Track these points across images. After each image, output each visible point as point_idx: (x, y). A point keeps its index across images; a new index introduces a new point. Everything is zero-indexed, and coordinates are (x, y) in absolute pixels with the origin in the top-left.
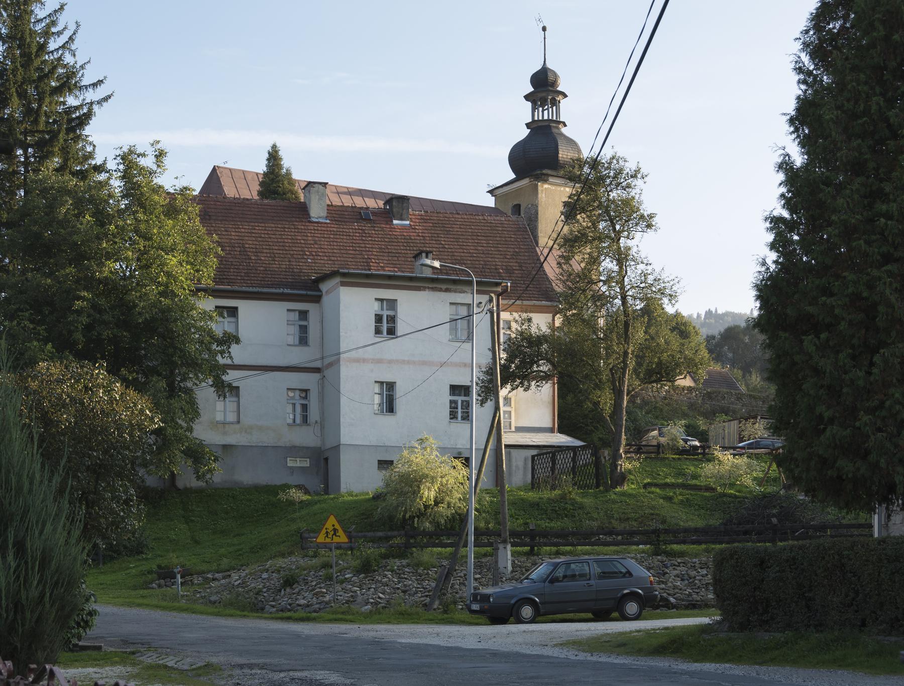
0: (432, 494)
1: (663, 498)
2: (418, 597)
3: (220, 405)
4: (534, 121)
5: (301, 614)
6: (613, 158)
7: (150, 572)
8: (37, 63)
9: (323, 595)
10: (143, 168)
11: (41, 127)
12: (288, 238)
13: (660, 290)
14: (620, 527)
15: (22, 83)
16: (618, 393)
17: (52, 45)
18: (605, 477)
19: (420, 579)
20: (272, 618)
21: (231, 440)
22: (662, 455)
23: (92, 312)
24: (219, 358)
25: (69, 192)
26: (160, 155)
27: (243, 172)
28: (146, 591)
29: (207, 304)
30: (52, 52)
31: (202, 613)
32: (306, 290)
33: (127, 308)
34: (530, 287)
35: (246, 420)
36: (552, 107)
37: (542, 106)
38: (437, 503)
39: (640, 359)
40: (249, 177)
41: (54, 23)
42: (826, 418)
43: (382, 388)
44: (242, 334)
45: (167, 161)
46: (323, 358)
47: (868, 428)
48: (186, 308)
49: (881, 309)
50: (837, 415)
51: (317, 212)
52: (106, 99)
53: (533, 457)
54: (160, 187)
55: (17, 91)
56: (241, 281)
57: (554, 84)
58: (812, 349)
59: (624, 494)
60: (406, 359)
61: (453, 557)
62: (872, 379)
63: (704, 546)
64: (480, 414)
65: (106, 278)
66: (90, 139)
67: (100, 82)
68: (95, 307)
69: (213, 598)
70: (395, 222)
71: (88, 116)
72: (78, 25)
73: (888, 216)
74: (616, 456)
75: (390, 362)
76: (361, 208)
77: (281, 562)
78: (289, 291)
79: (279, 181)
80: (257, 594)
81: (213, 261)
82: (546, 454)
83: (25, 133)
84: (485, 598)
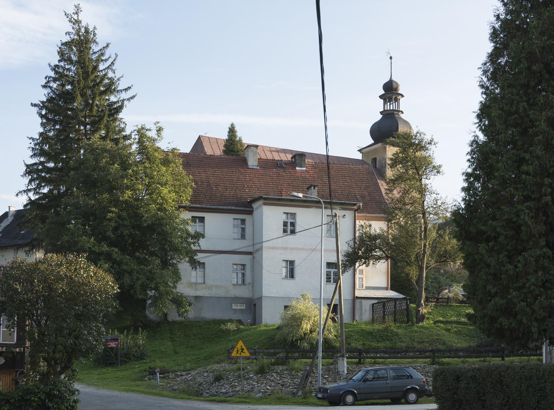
0: (309, 327)
1: (445, 330)
2: (290, 389)
3: (194, 273)
4: (384, 110)
5: (222, 398)
6: (417, 133)
7: (145, 371)
8: (92, 77)
9: (236, 387)
10: (149, 137)
11: (94, 113)
12: (232, 176)
13: (445, 209)
14: (418, 346)
15: (83, 89)
16: (421, 269)
17: (102, 67)
18: (410, 317)
19: (293, 377)
20: (207, 401)
21: (199, 293)
22: (450, 304)
23: (118, 219)
24: (192, 246)
25: (106, 151)
26: (159, 130)
27: (216, 139)
28: (140, 382)
29: (186, 215)
30: (102, 71)
31: (166, 396)
32: (244, 207)
33: (137, 216)
34: (377, 207)
35: (209, 282)
36: (395, 103)
37: (390, 101)
38: (311, 332)
39: (434, 248)
40: (219, 142)
41: (102, 54)
42: (493, 293)
43: (287, 264)
44: (208, 233)
45: (163, 133)
46: (253, 245)
47: (515, 299)
48: (172, 218)
49: (523, 228)
50: (499, 291)
51: (252, 162)
52: (133, 97)
53: (373, 304)
54: (159, 148)
55: (80, 93)
56: (206, 202)
57: (396, 89)
58: (484, 252)
59: (422, 327)
60: (301, 247)
61: (311, 365)
62: (518, 270)
63: (461, 359)
64: (345, 279)
65: (126, 200)
66: (123, 120)
67: (129, 88)
68: (119, 216)
69: (176, 387)
70: (297, 168)
71: (121, 107)
72: (117, 56)
73: (527, 173)
74: (419, 305)
75: (292, 249)
76: (278, 160)
77: (216, 367)
78: (234, 208)
79: (234, 145)
80: (200, 385)
81: (190, 191)
82: (382, 303)
83: (85, 117)
84: (325, 390)
